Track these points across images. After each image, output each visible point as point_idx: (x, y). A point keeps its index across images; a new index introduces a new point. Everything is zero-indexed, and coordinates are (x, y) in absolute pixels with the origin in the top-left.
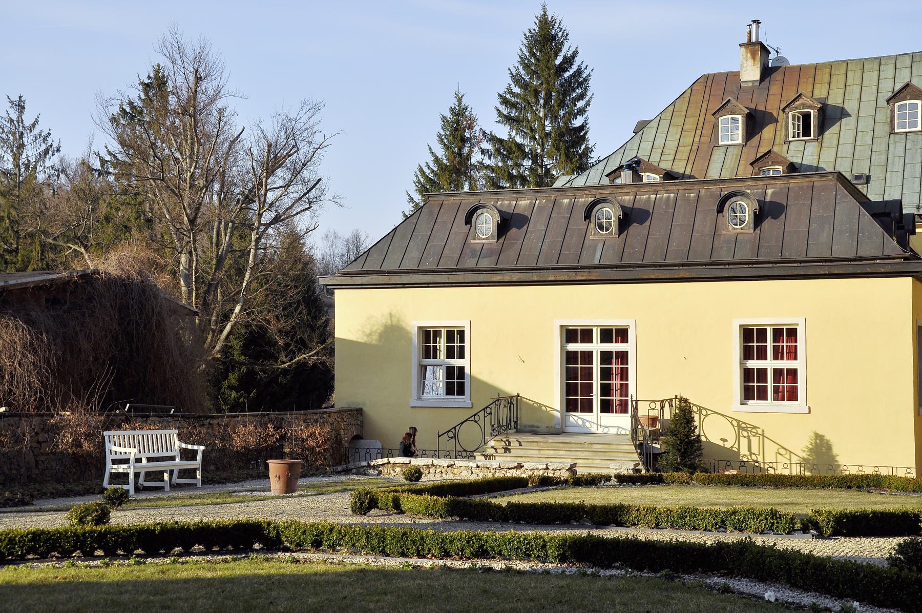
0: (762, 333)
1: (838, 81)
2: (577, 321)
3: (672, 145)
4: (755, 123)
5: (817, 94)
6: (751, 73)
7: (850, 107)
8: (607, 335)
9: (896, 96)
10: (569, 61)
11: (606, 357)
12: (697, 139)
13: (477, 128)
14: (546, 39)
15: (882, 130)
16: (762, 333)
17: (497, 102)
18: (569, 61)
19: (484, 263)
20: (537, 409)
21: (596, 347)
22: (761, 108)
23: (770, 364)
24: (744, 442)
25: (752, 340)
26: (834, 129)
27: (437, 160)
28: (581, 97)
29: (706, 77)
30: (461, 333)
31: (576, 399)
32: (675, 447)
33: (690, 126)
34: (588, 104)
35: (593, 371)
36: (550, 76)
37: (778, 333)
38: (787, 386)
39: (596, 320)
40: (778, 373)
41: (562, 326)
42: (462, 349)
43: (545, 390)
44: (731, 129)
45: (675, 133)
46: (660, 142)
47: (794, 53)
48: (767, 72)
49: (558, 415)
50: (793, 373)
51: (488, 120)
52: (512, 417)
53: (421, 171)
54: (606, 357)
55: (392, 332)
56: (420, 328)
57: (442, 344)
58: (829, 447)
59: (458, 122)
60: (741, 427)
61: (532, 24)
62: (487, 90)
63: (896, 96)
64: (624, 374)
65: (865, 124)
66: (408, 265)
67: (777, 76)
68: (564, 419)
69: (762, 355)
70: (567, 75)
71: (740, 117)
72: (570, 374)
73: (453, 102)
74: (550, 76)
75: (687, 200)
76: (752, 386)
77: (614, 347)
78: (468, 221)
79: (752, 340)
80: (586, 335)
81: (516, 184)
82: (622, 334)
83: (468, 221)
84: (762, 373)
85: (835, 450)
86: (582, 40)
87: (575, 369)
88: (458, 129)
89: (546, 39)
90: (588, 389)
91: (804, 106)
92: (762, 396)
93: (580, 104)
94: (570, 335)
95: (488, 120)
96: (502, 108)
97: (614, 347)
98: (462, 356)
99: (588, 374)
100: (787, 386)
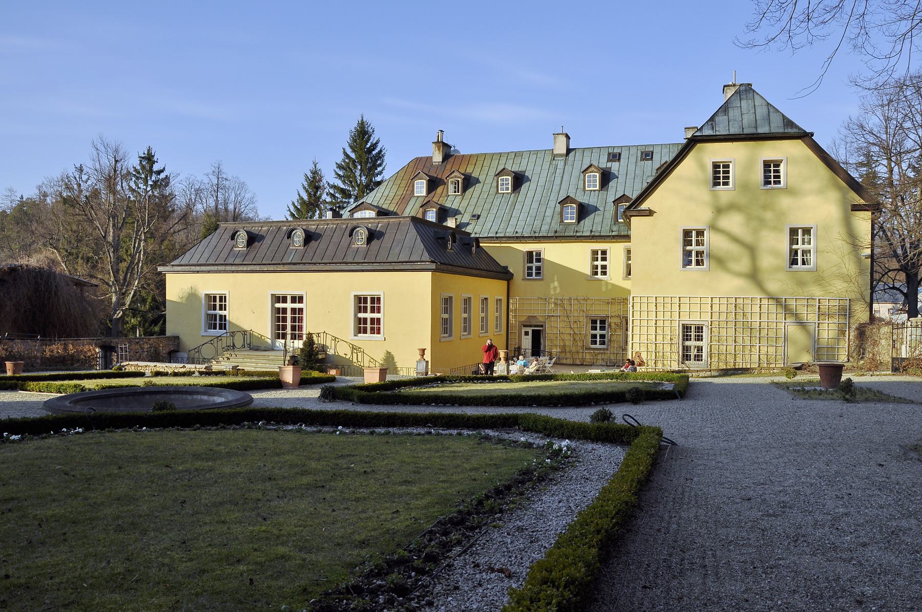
0: (365, 299)
1: (479, 163)
2: (280, 292)
3: (392, 195)
4: (433, 184)
5: (462, 171)
6: (438, 158)
7: (481, 178)
8: (294, 300)
9: (498, 175)
10: (374, 146)
13: (324, 181)
14: (362, 134)
15: (493, 190)
16: (365, 299)
17: (335, 166)
19: (238, 261)
20: (260, 338)
21: (289, 305)
22: (439, 177)
24: (355, 355)
25: (361, 302)
26: (471, 190)
27: (189, 207)
28: (380, 165)
29: (417, 159)
30: (379, 299)
31: (280, 333)
32: (312, 359)
33: (403, 185)
34: (383, 169)
35: (286, 317)
36: (364, 153)
37: (373, 300)
38: (375, 326)
39: (290, 292)
40: (372, 320)
43: (263, 328)
44: (421, 188)
45: (395, 188)
46: (386, 193)
47: (462, 147)
48: (447, 157)
49: (269, 341)
50: (379, 320)
51: (330, 177)
52: (253, 345)
53: (294, 204)
54: (294, 311)
55: (192, 296)
56: (206, 295)
57: (216, 302)
58: (393, 359)
59: (314, 178)
60: (354, 348)
61: (353, 125)
62: (331, 158)
63: (498, 175)
64: (301, 320)
65: (487, 187)
66: (202, 261)
67: (451, 160)
68: (273, 343)
69: (365, 311)
70: (374, 153)
72: (278, 319)
73: (312, 167)
74: (364, 153)
75: (341, 229)
76: (361, 327)
77: (297, 306)
78: (351, 235)
79: (361, 302)
80: (284, 300)
82: (300, 299)
83: (351, 235)
84: (365, 320)
85: (396, 360)
86: (381, 136)
87: (279, 316)
88: (314, 183)
89: (362, 134)
90: (284, 328)
91: (456, 177)
92: (365, 332)
93: (379, 169)
94: (277, 299)
95: (330, 177)
96: (337, 170)
97: (297, 306)
98: (379, 312)
99: (285, 320)
100: (375, 326)
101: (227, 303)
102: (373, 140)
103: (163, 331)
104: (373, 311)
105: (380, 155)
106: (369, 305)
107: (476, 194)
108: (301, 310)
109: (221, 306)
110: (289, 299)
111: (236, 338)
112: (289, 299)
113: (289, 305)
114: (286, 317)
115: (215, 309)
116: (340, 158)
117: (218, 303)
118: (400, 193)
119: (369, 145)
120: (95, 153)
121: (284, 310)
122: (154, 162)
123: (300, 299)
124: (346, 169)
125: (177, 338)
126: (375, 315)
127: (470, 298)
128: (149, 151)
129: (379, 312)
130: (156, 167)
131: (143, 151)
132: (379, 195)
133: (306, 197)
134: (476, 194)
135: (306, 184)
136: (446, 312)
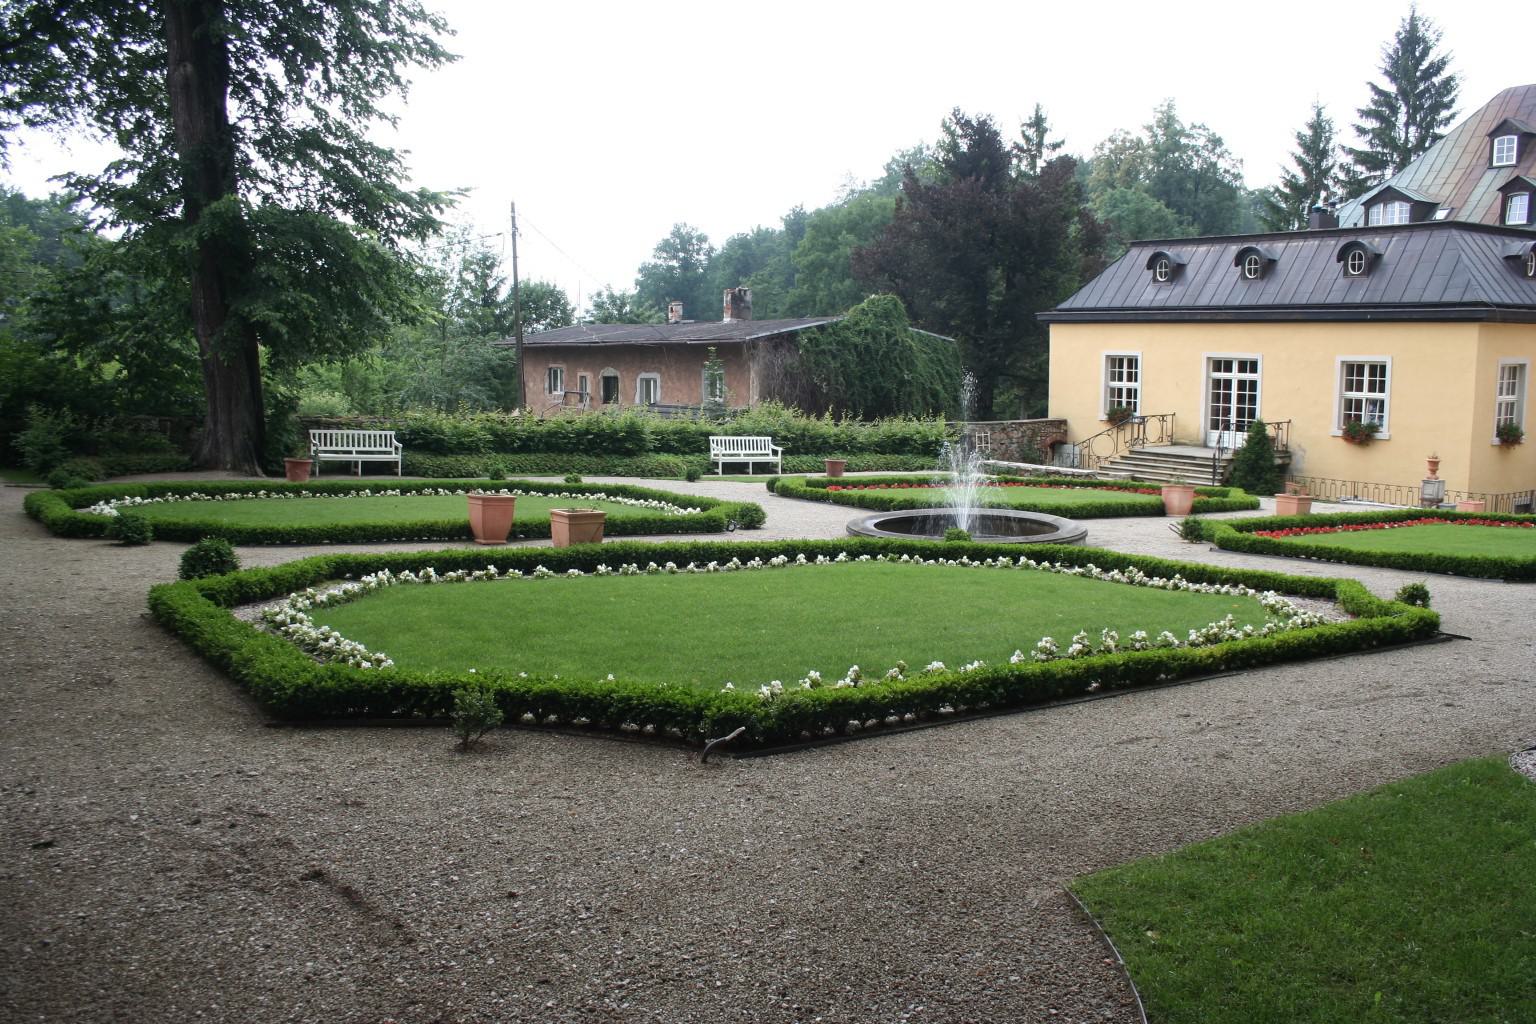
2: (1223, 354)
10: (1437, 68)
11: (1242, 384)
12: (1475, 161)
14: (1412, 43)
18: (1437, 68)
23: (1365, 394)
28: (1448, 106)
30: (1383, 368)
31: (1219, 422)
41: (1343, 362)
42: (1383, 383)
54: (1242, 384)
61: (1388, 40)
64: (1253, 399)
69: (1360, 389)
71: (1516, 138)
72: (1216, 398)
73: (1311, 117)
77: (1248, 376)
79: (1353, 370)
81: (199, 244)
82: (1253, 366)
89: (1412, 43)
93: (1444, 114)
97: (1248, 376)
98: (1382, 390)
99: (1227, 398)
101: (1139, 370)
102: (1433, 57)
103: (1044, 412)
104: (1372, 389)
105: (1448, 85)
106: (1366, 378)
107: (1122, 272)
108: (1253, 384)
109: (1130, 375)
110: (1235, 366)
111: (1148, 425)
112: (1235, 366)
113: (1235, 376)
114: (1233, 394)
115: (1121, 379)
116: (1367, 100)
117: (1125, 370)
118: (1464, 163)
119: (1425, 65)
120: (948, 139)
121: (1228, 384)
122: (1045, 130)
123: (1253, 366)
124: (1382, 110)
125: (1064, 422)
126: (1132, 385)
127: (1523, 367)
128: (1037, 112)
129: (1382, 390)
130: (1048, 139)
131: (1029, 115)
132: (1424, 169)
133: (1302, 178)
134: (1122, 272)
135: (1299, 151)
136: (1512, 390)
